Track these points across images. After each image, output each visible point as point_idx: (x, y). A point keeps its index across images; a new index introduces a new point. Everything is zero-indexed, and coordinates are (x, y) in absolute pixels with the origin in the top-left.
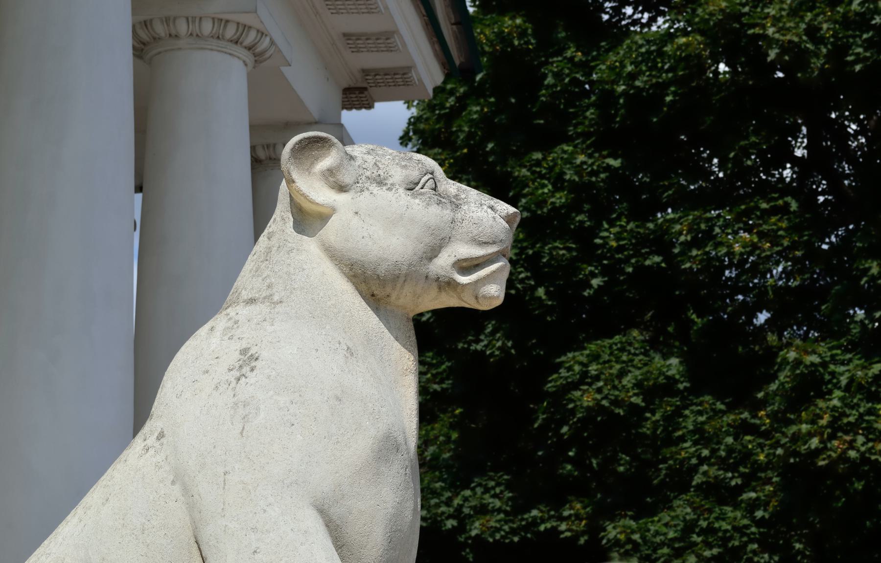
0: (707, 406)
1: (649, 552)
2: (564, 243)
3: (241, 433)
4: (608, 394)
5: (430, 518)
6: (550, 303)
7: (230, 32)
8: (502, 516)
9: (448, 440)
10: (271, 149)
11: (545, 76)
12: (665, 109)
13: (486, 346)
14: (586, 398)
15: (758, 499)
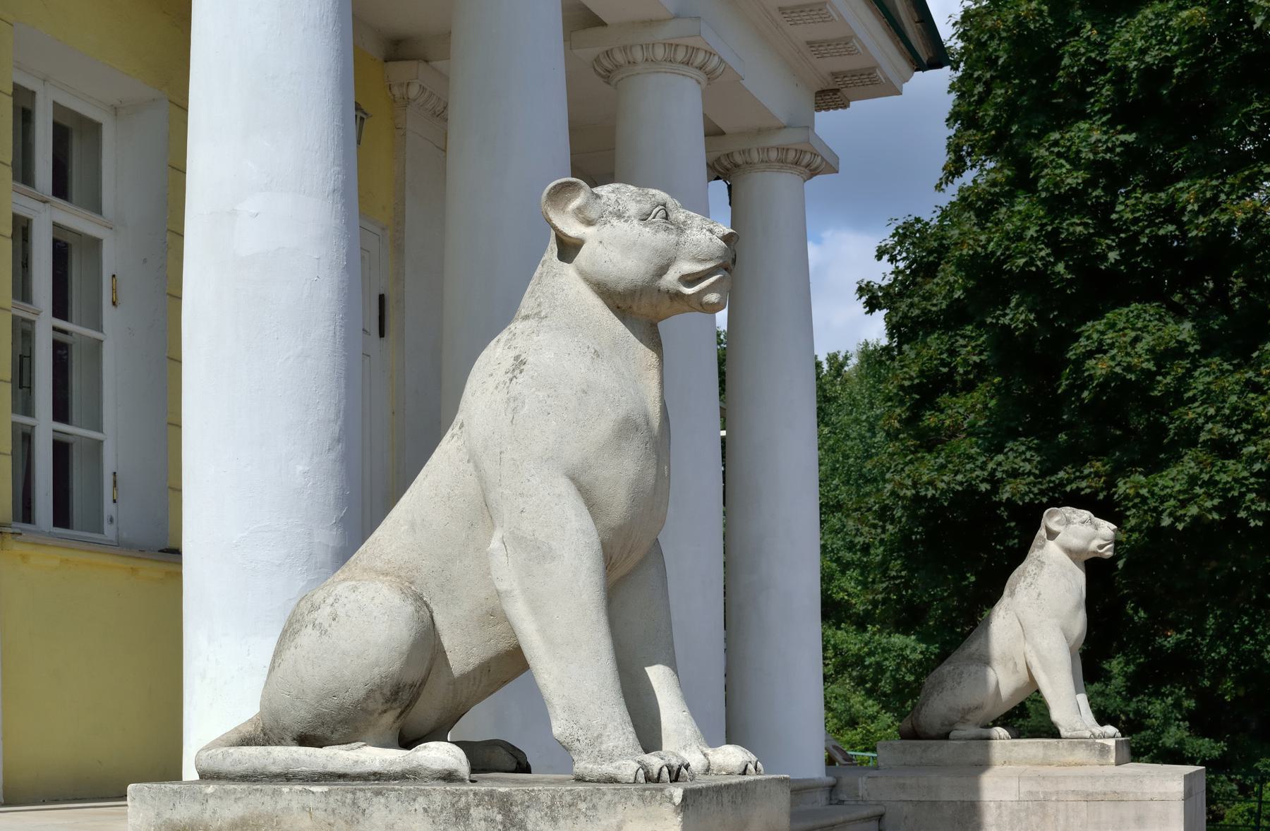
0: (1214, 366)
1: (1157, 504)
2: (1081, 219)
3: (512, 422)
4: (1121, 361)
5: (966, 482)
6: (1069, 277)
7: (681, 55)
8: (1032, 478)
9: (986, 407)
10: (747, 155)
11: (1061, 57)
12: (1174, 81)
13: (1012, 319)
14: (1099, 367)
15: (1256, 452)
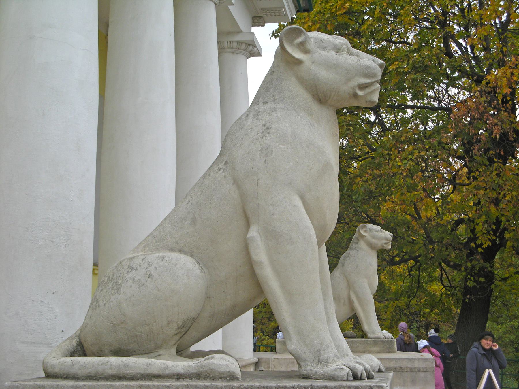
10: (222, 43)
